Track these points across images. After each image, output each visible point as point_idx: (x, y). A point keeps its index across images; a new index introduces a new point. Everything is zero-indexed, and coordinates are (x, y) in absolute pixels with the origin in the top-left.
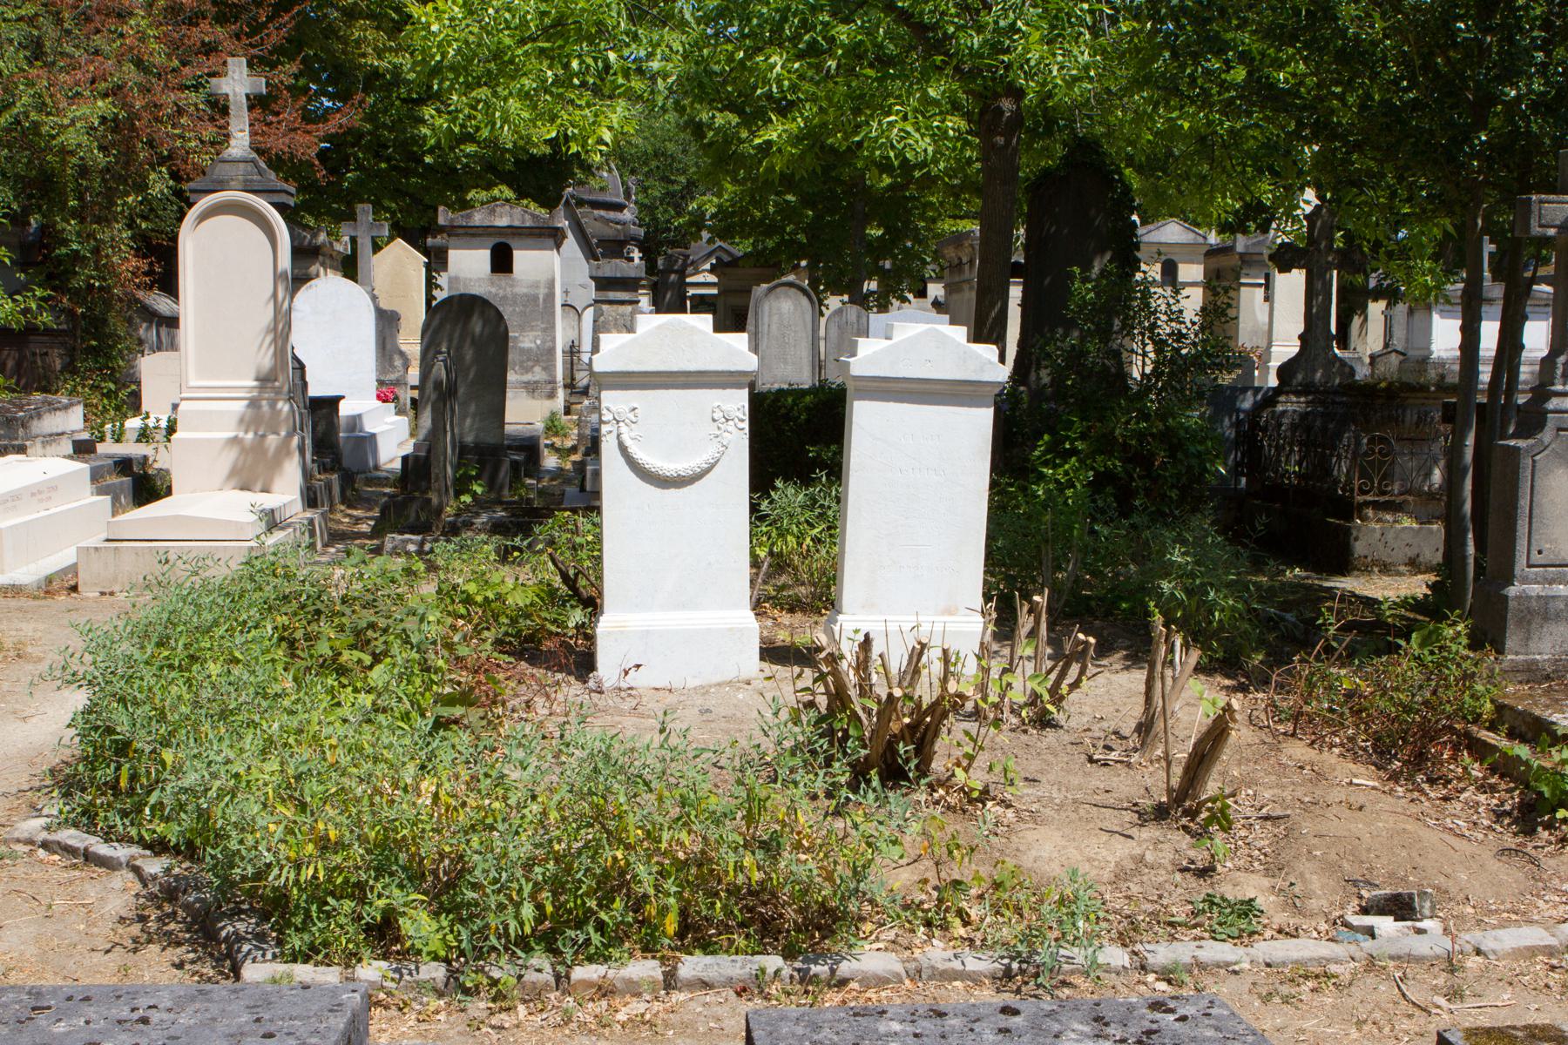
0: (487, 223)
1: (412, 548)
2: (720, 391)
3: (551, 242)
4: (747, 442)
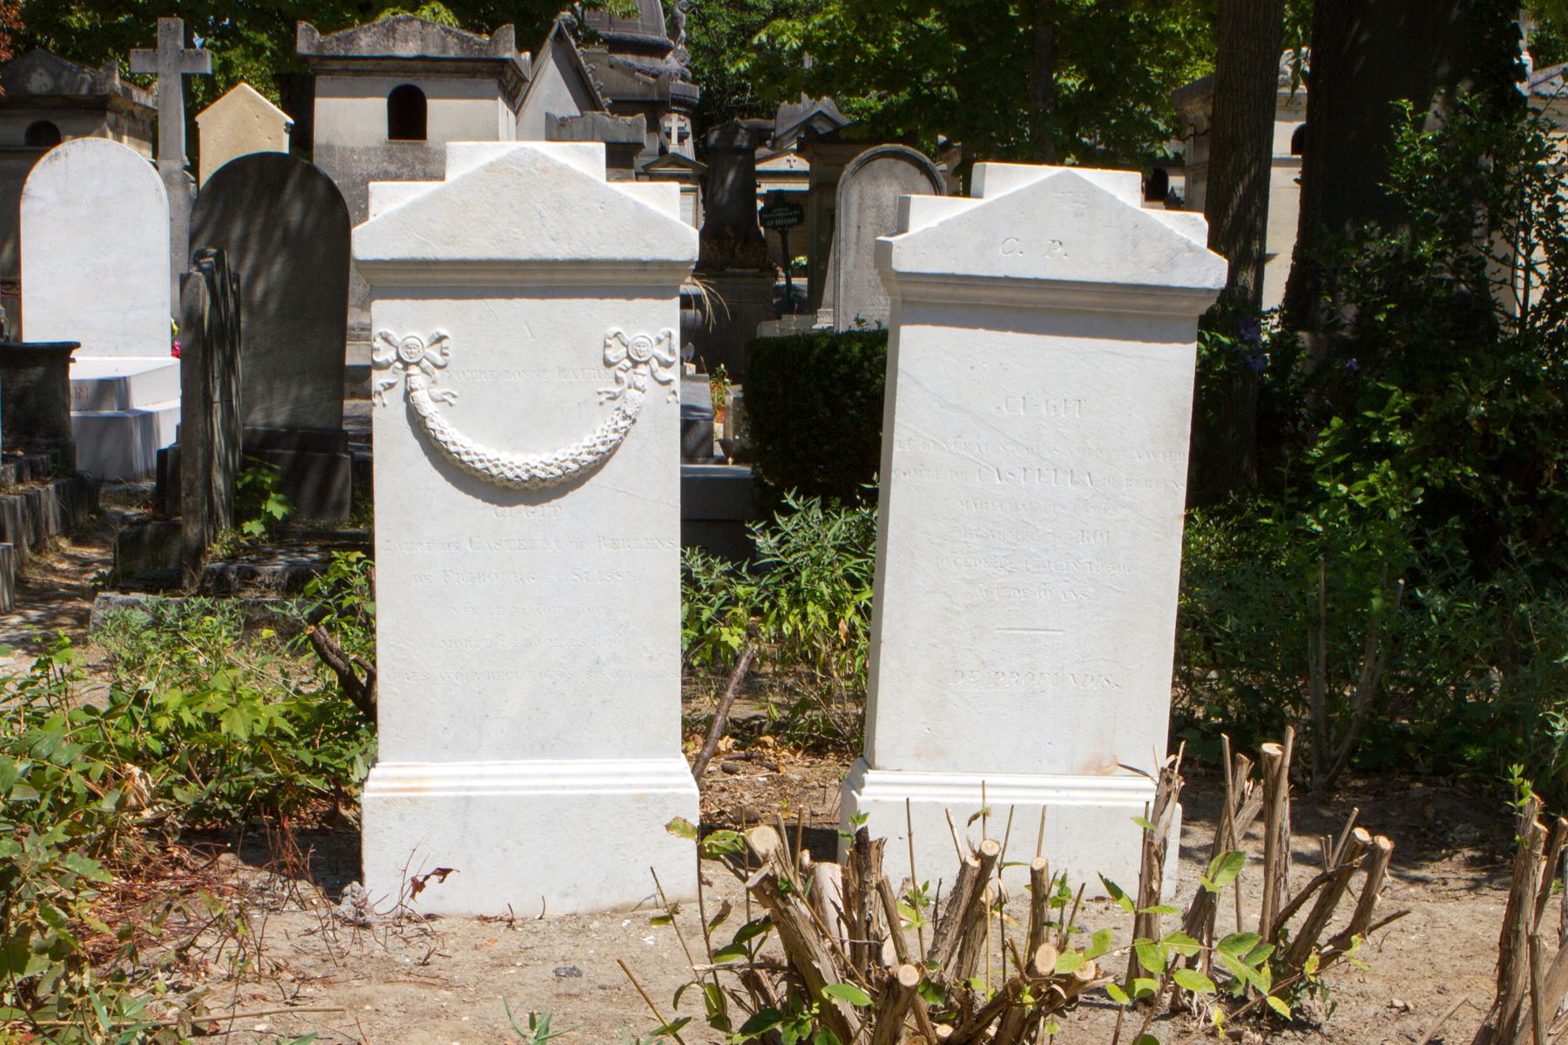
1: (140, 617)
2: (596, 302)
3: (492, 84)
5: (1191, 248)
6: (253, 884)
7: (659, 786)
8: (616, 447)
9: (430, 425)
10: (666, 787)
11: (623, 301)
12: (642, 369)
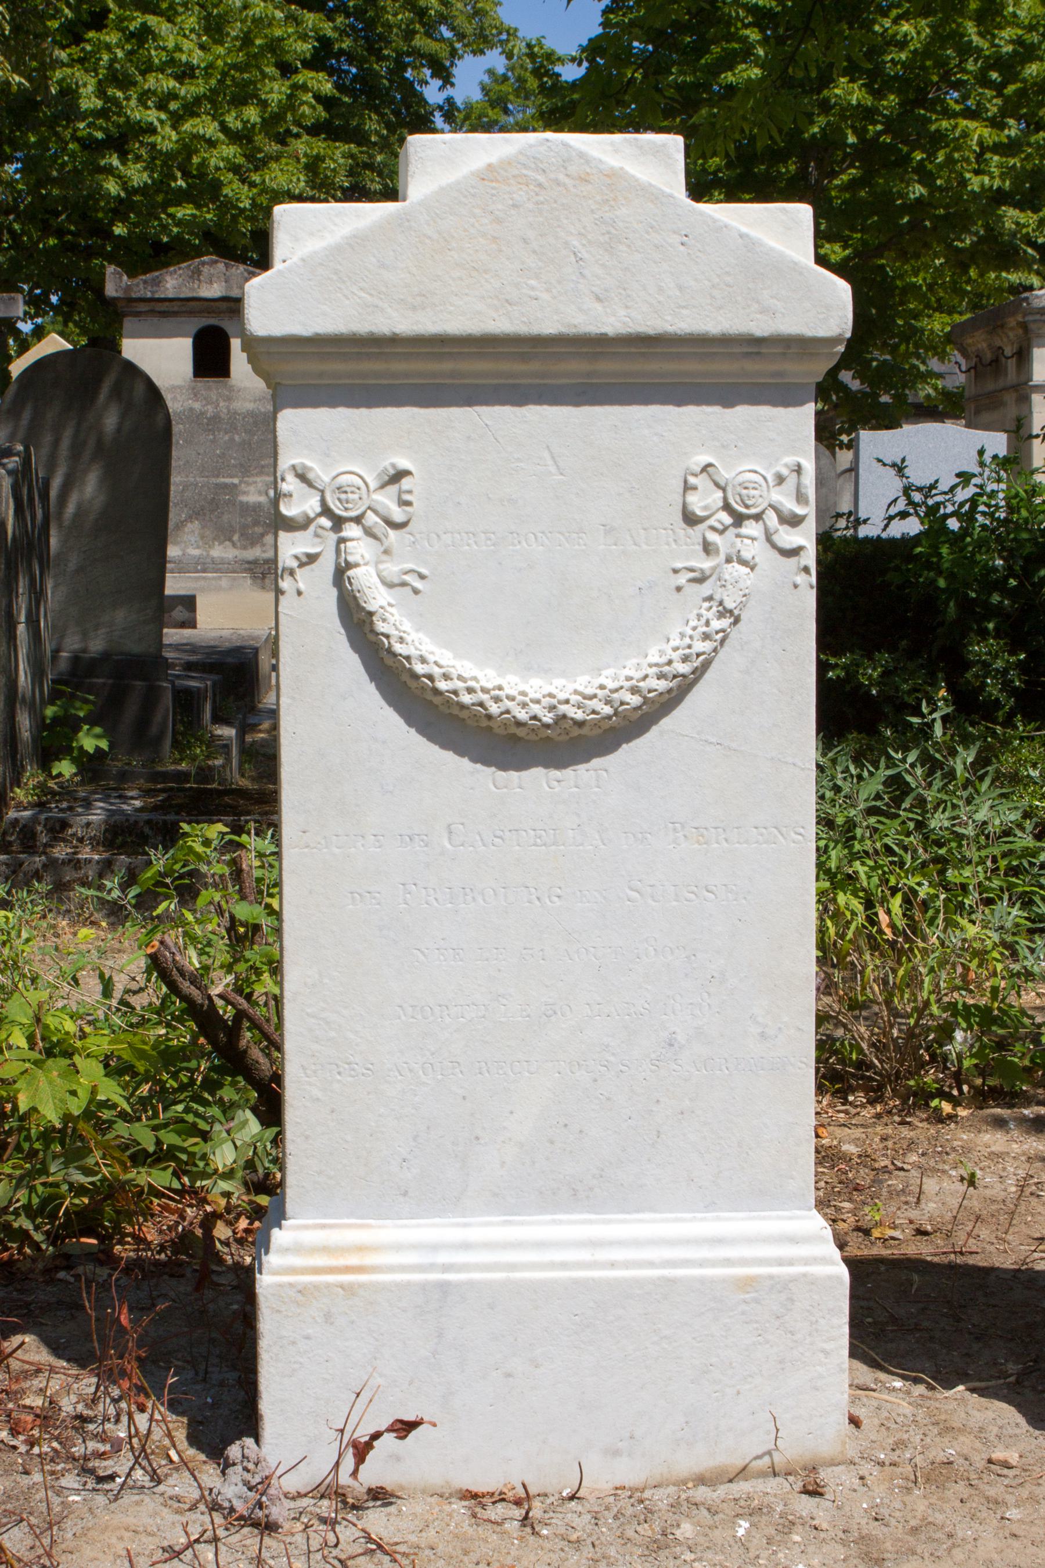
0: (186, 293)
4: (809, 601)
6: (68, 1405)
7: (780, 1262)
8: (706, 665)
9: (381, 627)
10: (791, 1262)
11: (717, 409)
12: (751, 528)
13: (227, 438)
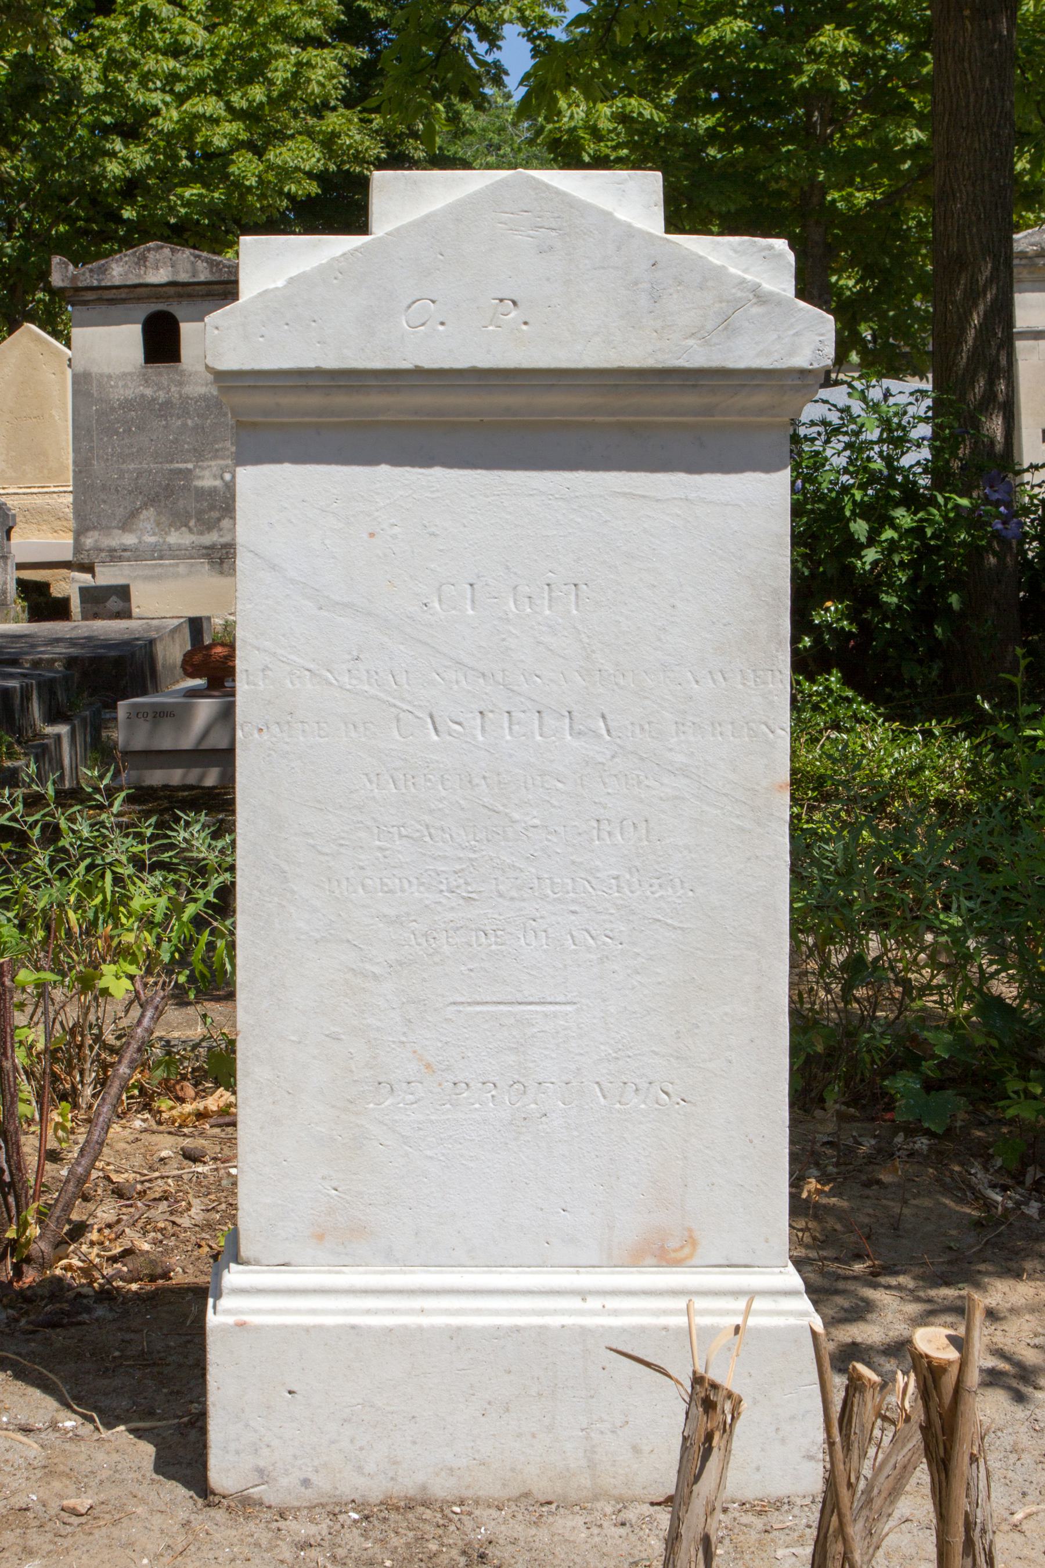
0: (133, 280)
5: (760, 297)
13: (179, 423)
